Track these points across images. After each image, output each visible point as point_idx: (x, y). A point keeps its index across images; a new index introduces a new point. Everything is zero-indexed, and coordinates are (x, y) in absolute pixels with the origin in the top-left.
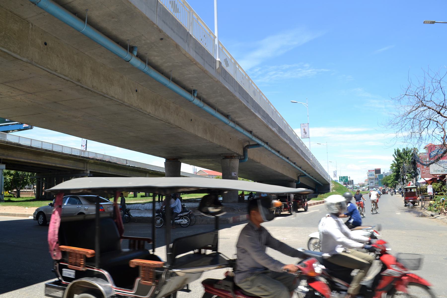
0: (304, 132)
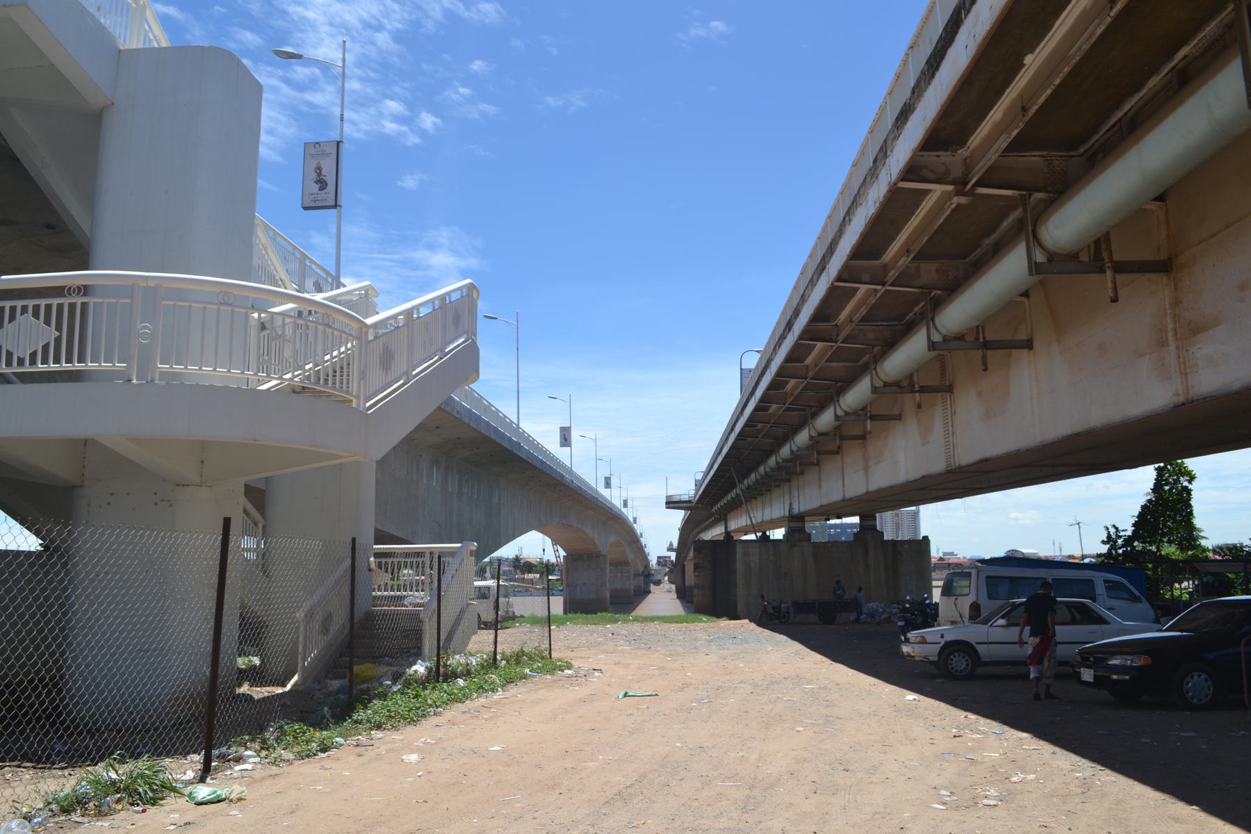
0: (317, 182)
